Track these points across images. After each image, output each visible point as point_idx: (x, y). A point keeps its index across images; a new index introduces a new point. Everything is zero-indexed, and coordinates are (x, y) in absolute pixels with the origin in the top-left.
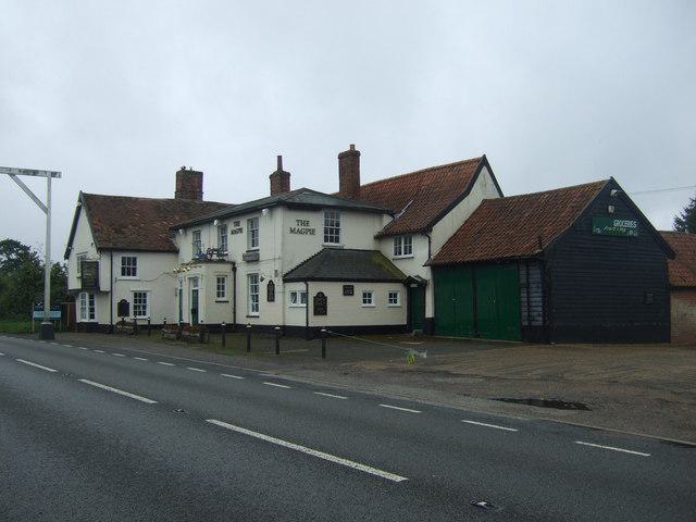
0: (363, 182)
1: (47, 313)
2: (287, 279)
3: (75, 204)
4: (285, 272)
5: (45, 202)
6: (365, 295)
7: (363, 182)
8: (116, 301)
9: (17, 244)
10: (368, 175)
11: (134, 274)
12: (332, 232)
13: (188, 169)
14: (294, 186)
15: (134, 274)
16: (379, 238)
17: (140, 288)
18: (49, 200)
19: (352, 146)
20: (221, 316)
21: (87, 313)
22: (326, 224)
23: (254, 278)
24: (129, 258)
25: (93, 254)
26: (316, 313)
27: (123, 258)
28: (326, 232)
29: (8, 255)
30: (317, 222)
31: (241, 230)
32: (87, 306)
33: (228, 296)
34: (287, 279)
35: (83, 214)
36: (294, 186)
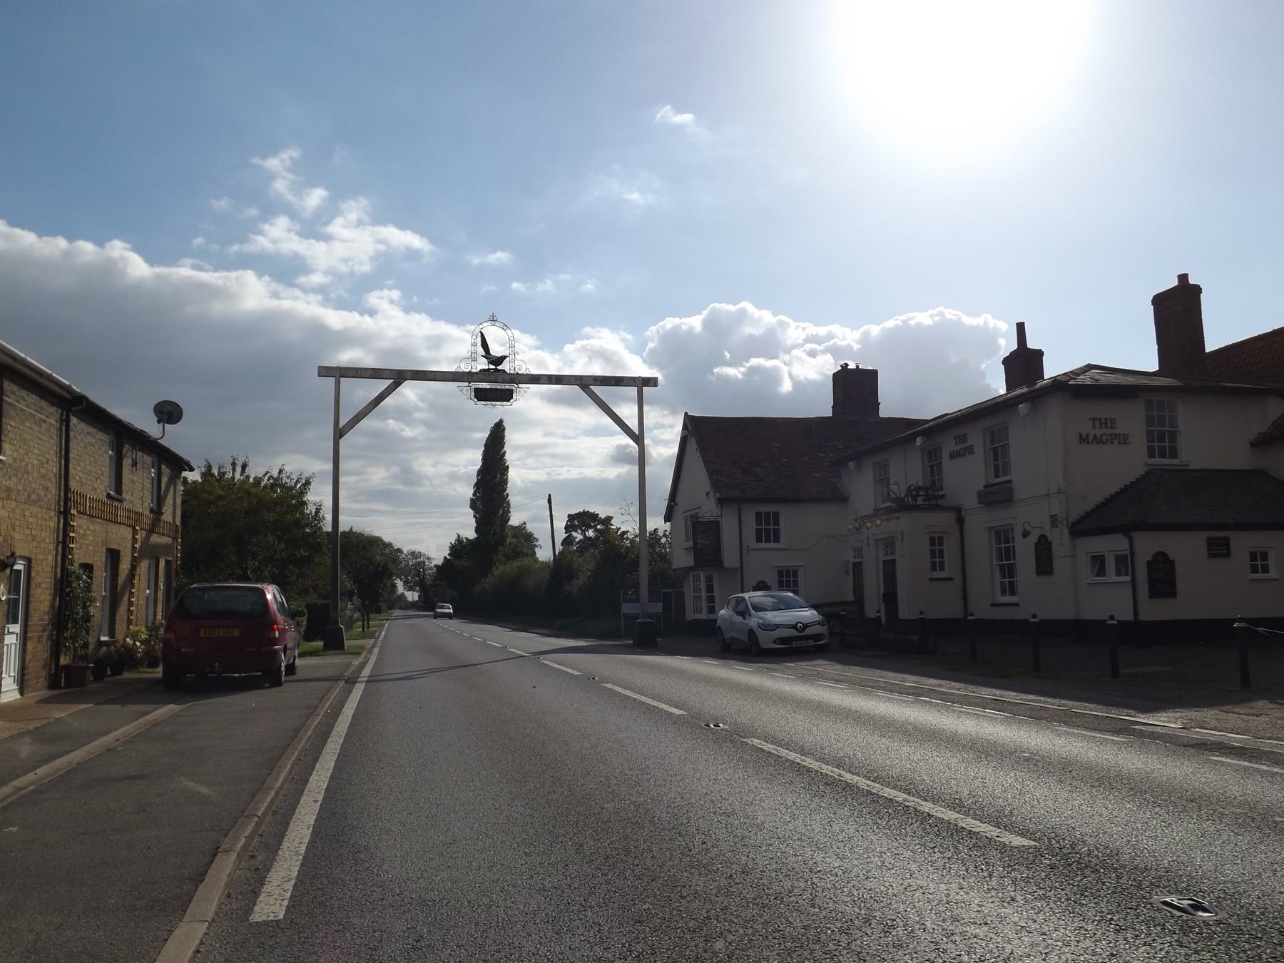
0: (1211, 345)
1: (639, 606)
2: (1082, 528)
4: (1074, 517)
5: (635, 429)
6: (1253, 556)
7: (1211, 345)
9: (594, 517)
10: (1217, 336)
11: (777, 540)
12: (1161, 437)
13: (852, 366)
14: (1052, 368)
15: (777, 540)
16: (1261, 443)
19: (1183, 278)
20: (944, 606)
21: (704, 605)
22: (1150, 421)
23: (1003, 536)
24: (767, 514)
25: (709, 509)
26: (1155, 593)
27: (758, 515)
28: (1150, 440)
29: (583, 532)
30: (1132, 420)
31: (970, 450)
32: (704, 594)
33: (952, 568)
34: (1082, 528)
36: (1052, 368)
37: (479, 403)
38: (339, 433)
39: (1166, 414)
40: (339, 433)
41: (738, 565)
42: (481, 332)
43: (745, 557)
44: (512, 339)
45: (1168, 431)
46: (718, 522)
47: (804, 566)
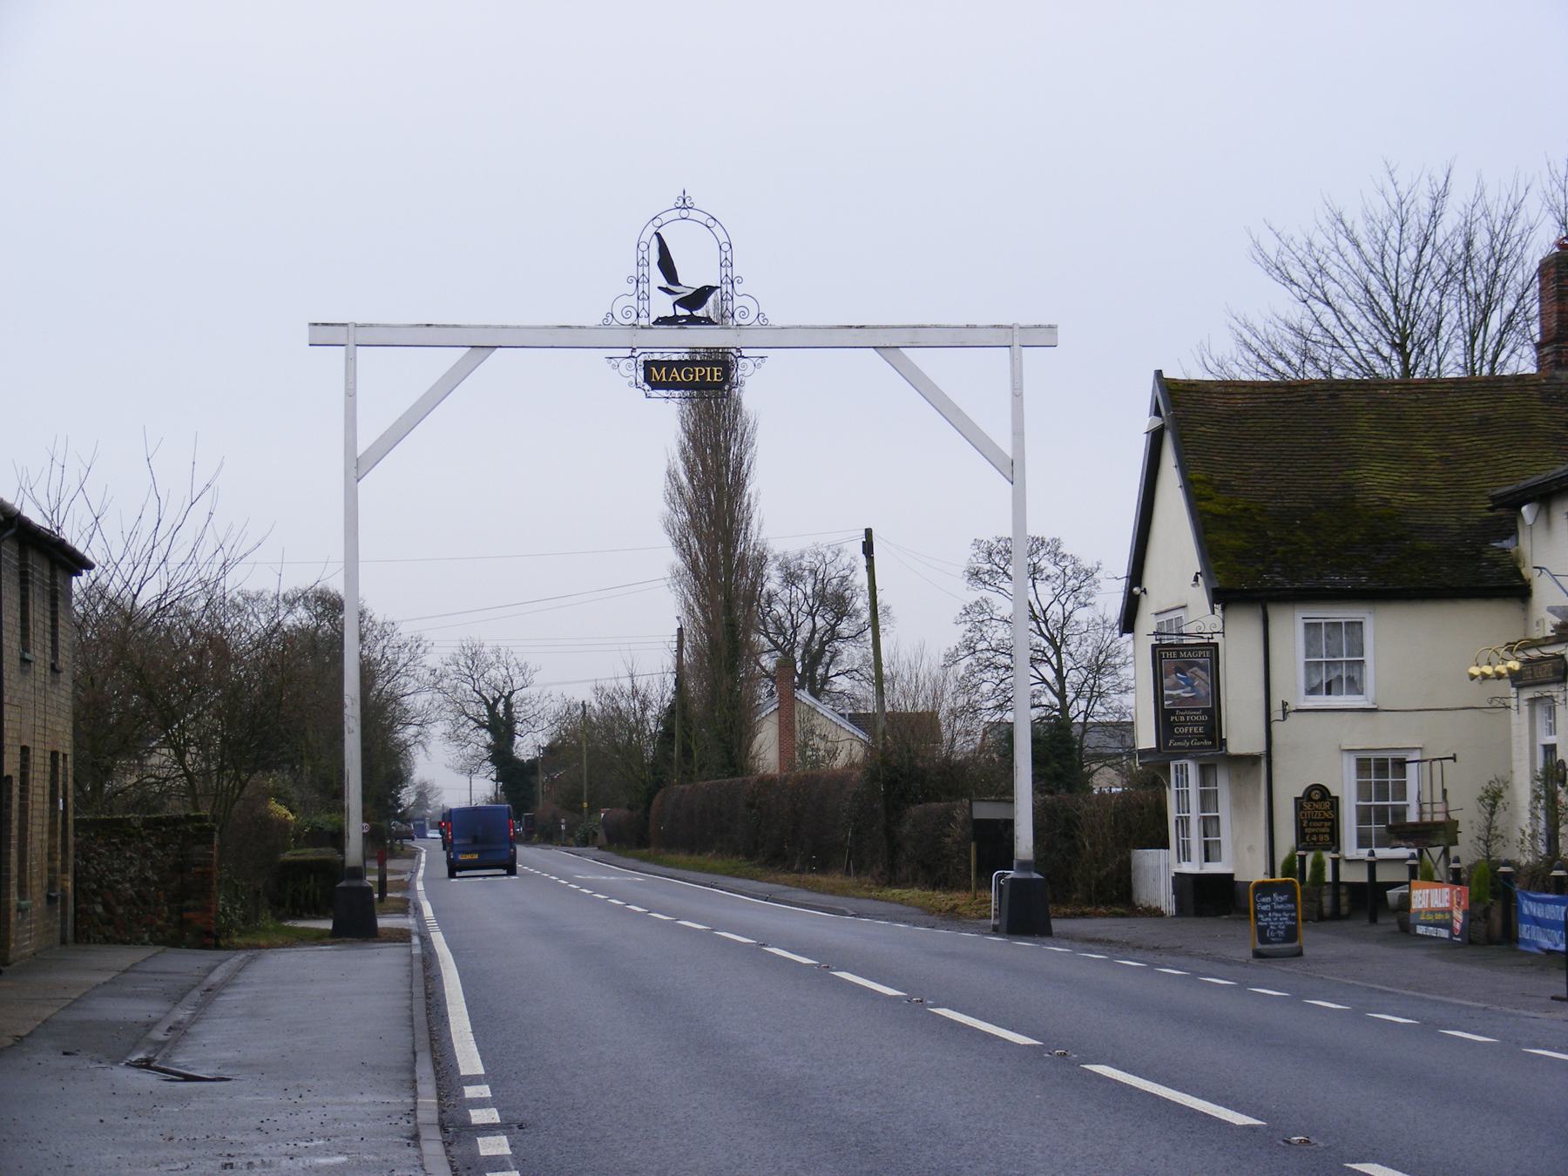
3: (1144, 421)
5: (1006, 447)
8: (1289, 789)
11: (1355, 686)
15: (1355, 686)
17: (1382, 736)
18: (1018, 433)
25: (1201, 617)
35: (1443, 856)
37: (654, 393)
38: (357, 467)
39: (1390, 780)
40: (357, 467)
41: (1258, 747)
42: (658, 235)
43: (1275, 727)
44: (725, 247)
45: (1391, 805)
46: (1216, 645)
47: (1420, 748)
